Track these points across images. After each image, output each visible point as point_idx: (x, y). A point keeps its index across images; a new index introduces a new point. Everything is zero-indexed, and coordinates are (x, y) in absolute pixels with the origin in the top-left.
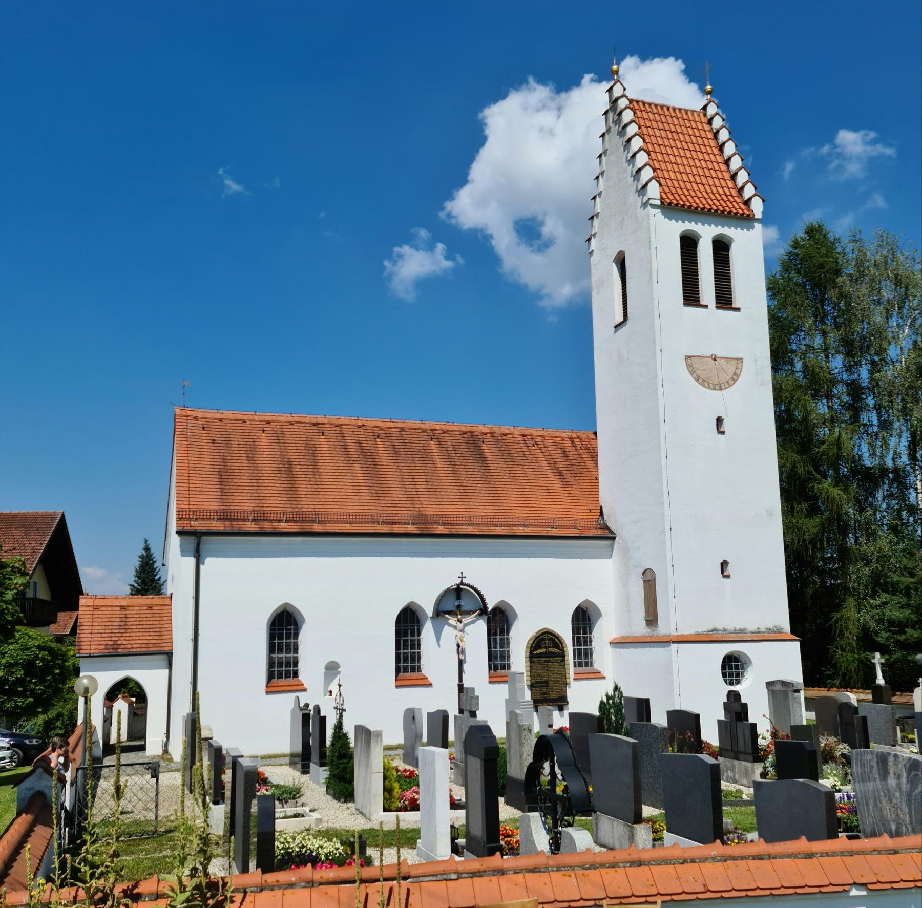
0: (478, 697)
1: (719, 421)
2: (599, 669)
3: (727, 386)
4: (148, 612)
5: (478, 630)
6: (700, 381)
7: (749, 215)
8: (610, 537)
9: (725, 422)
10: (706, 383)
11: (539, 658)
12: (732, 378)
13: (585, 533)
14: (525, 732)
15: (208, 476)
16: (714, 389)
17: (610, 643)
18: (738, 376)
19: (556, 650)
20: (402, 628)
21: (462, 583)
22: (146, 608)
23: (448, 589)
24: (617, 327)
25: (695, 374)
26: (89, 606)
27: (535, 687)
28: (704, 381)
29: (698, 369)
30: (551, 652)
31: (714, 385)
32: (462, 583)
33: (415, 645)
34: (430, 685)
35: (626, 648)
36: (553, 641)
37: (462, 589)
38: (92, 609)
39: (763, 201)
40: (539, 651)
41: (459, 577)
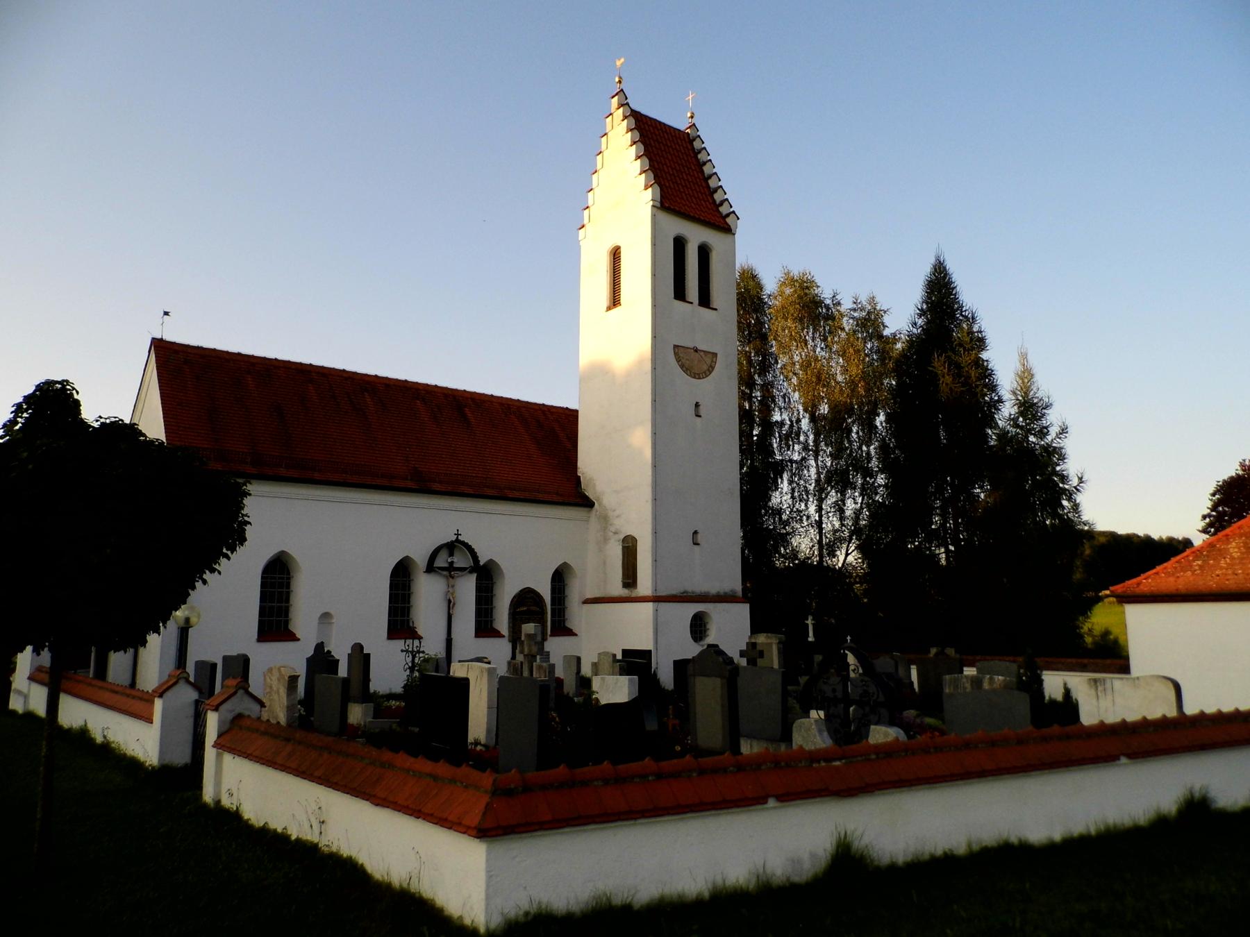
0: (549, 652)
1: (697, 405)
5: (467, 587)
9: (701, 407)
10: (689, 372)
12: (708, 370)
16: (695, 377)
18: (713, 368)
21: (457, 540)
25: (680, 362)
31: (695, 374)
32: (457, 540)
34: (299, 640)
41: (455, 534)
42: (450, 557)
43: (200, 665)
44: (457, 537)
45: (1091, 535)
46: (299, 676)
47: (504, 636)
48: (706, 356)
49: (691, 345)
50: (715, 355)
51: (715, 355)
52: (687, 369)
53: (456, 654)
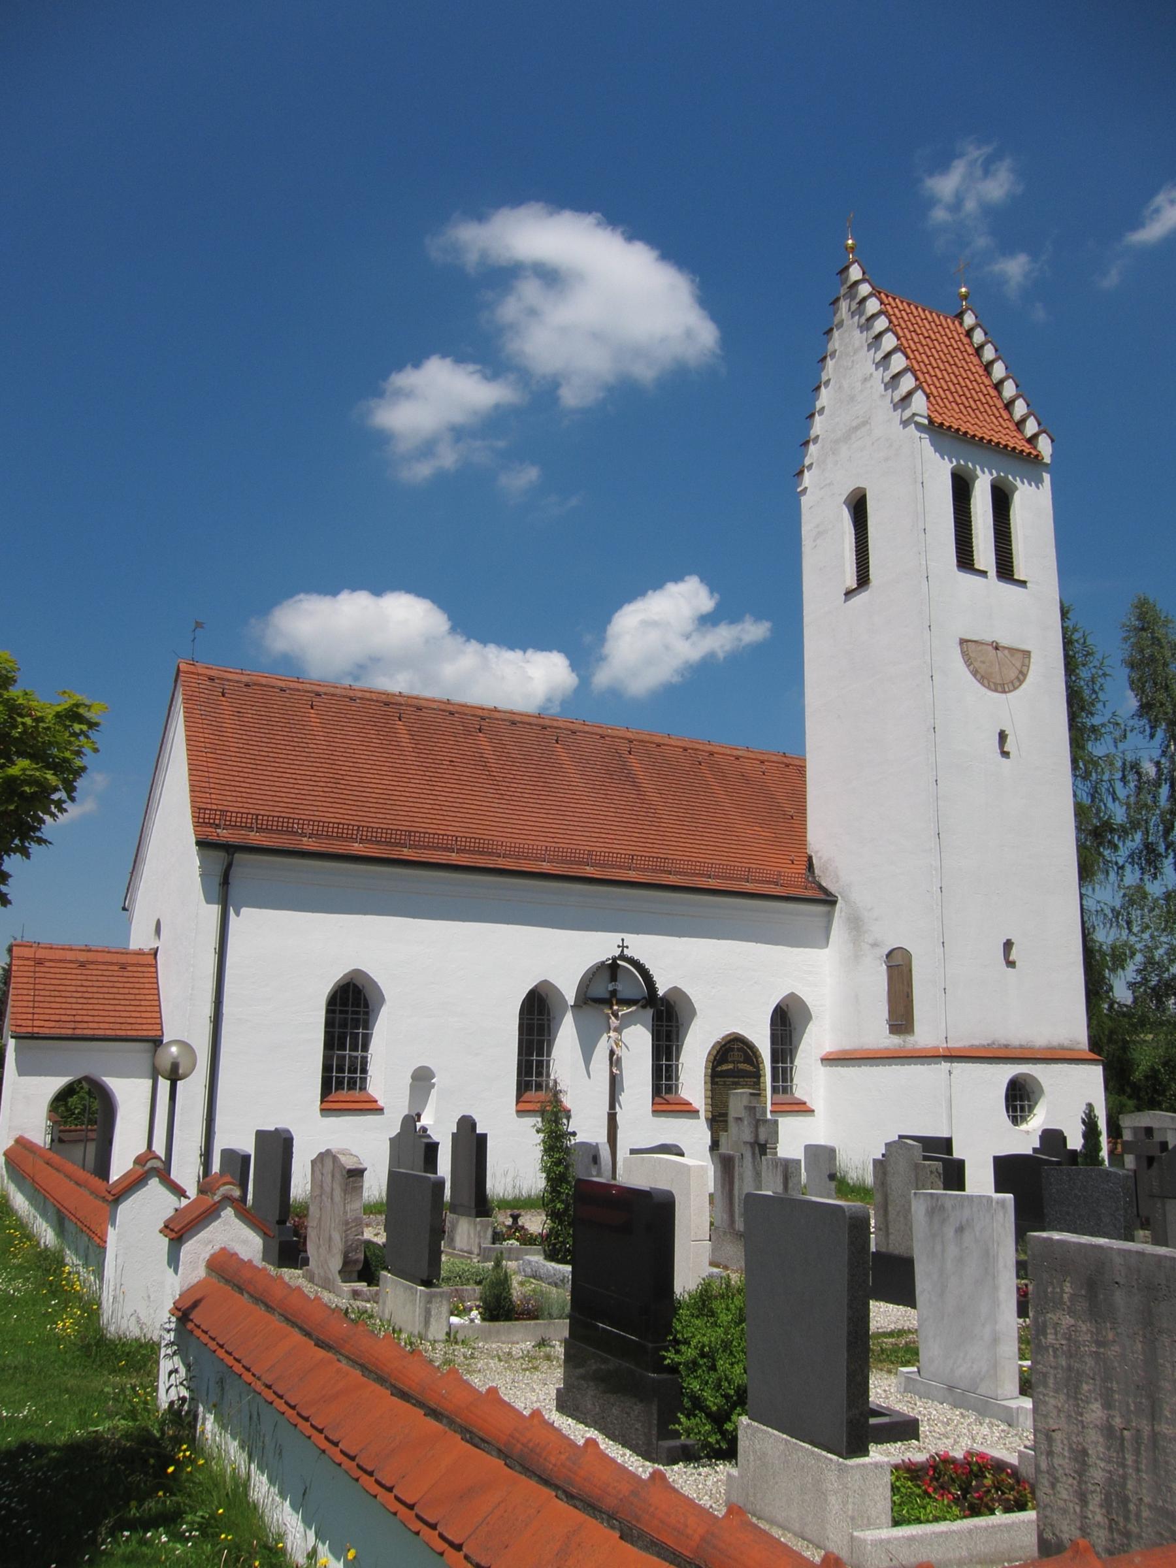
2: (804, 1098)
3: (1011, 688)
4: (121, 974)
6: (979, 676)
7: (1037, 456)
8: (828, 900)
11: (724, 1077)
12: (1018, 678)
13: (792, 892)
14: (933, 1176)
15: (235, 764)
16: (996, 691)
17: (822, 1060)
18: (1025, 675)
19: (751, 1068)
20: (536, 1022)
21: (622, 957)
22: (116, 968)
23: (603, 963)
24: (849, 594)
25: (972, 667)
26: (28, 959)
27: (717, 1121)
28: (982, 677)
29: (976, 660)
30: (742, 1070)
31: (995, 684)
32: (622, 957)
33: (343, 1083)
35: (853, 1066)
36: (746, 1053)
37: (619, 965)
38: (33, 963)
39: (1052, 441)
40: (725, 1067)
41: (619, 946)
42: (611, 982)
43: (228, 1154)
44: (622, 951)
45: (578, 675)
46: (366, 1169)
47: (694, 1113)
48: (1012, 655)
49: (988, 638)
50: (1027, 654)
51: (1027, 654)
52: (982, 677)
53: (625, 1143)
